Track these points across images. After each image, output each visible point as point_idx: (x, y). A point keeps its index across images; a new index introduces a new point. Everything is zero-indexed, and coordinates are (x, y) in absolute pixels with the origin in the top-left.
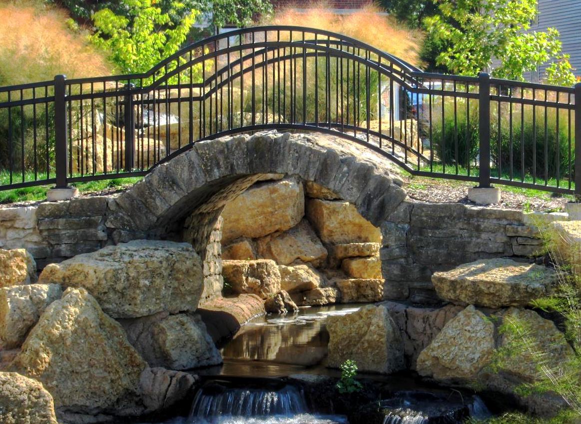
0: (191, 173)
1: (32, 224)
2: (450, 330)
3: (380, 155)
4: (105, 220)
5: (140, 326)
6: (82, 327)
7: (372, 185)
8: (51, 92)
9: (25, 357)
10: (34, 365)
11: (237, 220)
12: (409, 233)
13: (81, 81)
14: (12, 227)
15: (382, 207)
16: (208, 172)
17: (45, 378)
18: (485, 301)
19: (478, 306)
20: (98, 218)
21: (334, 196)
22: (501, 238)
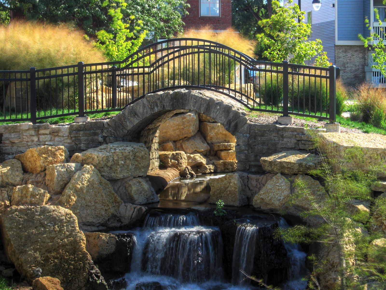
0: (144, 109)
1: (67, 134)
2: (269, 185)
4: (102, 132)
5: (119, 183)
7: (231, 115)
8: (76, 71)
10: (68, 202)
11: (166, 132)
12: (249, 138)
13: (91, 65)
15: (236, 126)
16: (152, 109)
17: (73, 208)
18: (286, 171)
19: (283, 174)
20: (99, 131)
22: (294, 141)
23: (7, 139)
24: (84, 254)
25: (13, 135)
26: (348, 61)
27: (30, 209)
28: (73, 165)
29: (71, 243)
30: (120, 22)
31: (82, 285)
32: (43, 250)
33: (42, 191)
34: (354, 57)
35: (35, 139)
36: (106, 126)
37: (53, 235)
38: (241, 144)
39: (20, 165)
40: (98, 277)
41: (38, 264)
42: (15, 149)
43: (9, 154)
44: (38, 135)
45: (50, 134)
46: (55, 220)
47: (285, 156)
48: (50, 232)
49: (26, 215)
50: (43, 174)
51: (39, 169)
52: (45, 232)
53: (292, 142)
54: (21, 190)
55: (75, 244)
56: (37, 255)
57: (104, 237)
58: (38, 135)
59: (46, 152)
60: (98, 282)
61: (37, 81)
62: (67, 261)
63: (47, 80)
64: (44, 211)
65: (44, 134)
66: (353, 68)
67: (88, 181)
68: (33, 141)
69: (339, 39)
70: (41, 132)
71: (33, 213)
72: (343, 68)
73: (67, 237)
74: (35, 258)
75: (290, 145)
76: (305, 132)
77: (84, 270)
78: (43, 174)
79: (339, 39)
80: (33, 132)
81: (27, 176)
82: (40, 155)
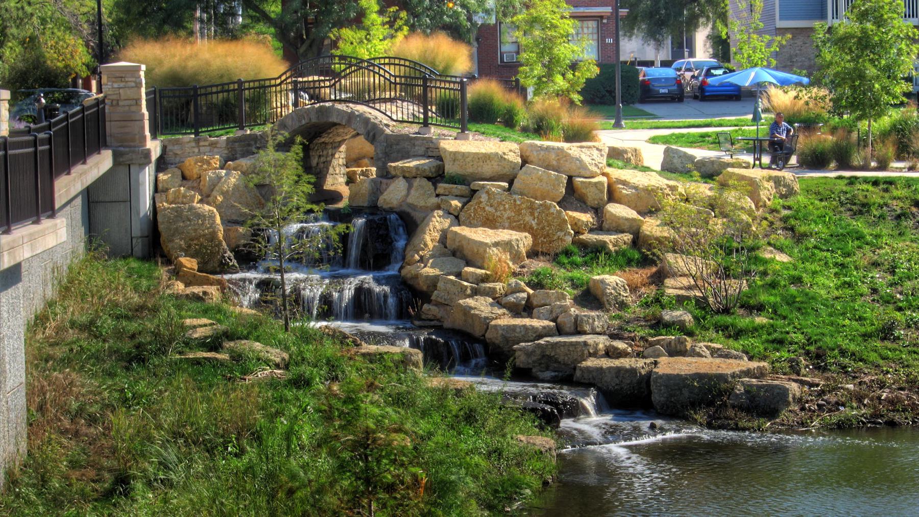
0: (292, 121)
1: (224, 145)
2: (391, 188)
3: (696, 124)
4: (256, 143)
5: (266, 189)
6: (236, 187)
7: (370, 126)
8: (236, 87)
9: (210, 199)
10: (215, 202)
11: (362, 148)
12: (387, 147)
13: (270, 79)
14: (216, 147)
15: (374, 136)
16: (300, 121)
17: (218, 208)
18: (407, 175)
19: (404, 177)
20: (253, 143)
21: (583, 150)
22: (423, 149)
23: (171, 151)
24: (220, 242)
25: (176, 147)
26: (798, 52)
27: (180, 207)
28: (223, 172)
29: (211, 234)
30: (374, 16)
31: (216, 265)
32: (187, 240)
33: (193, 193)
34: (807, 45)
35: (196, 150)
36: (259, 138)
37: (196, 227)
38: (379, 152)
39: (180, 173)
40: (231, 260)
41: (182, 249)
42: (177, 160)
43: (172, 164)
44: (198, 146)
45: (209, 145)
46: (199, 216)
47: (409, 162)
48: (194, 225)
49: (177, 212)
50: (198, 180)
51: (195, 176)
52: (190, 225)
53: (421, 150)
54: (175, 192)
55: (213, 236)
56: (182, 243)
57: (241, 230)
58: (198, 146)
59: (202, 161)
60: (231, 264)
61: (199, 98)
62: (205, 247)
63: (225, 94)
64: (191, 209)
65: (204, 146)
66: (806, 63)
67: (234, 185)
68: (194, 152)
69: (781, 19)
70: (202, 143)
71: (182, 210)
72: (789, 64)
73: (208, 229)
74: (181, 245)
75: (420, 152)
76: (434, 141)
77: (218, 254)
78: (198, 180)
79: (781, 19)
80: (193, 144)
81: (185, 182)
82: (196, 163)
